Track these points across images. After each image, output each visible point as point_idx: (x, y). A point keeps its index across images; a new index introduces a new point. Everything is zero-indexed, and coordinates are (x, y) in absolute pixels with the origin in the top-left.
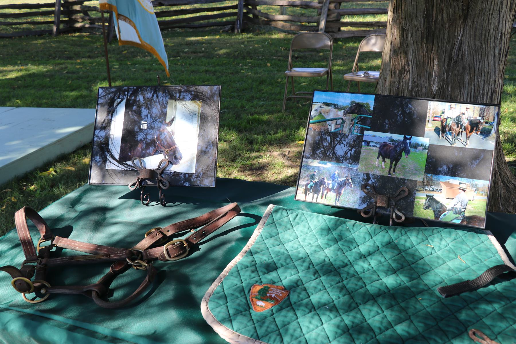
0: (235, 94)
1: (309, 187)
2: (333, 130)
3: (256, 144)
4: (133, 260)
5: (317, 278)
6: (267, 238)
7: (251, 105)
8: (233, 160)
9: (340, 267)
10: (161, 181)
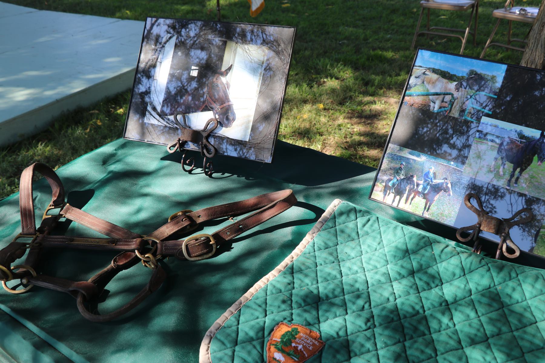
0: (360, 23)
1: (390, 184)
2: (436, 109)
3: (372, 86)
4: (142, 253)
5: (369, 328)
6: (320, 249)
7: (376, 37)
8: (341, 103)
9: (408, 315)
10: (206, 147)
